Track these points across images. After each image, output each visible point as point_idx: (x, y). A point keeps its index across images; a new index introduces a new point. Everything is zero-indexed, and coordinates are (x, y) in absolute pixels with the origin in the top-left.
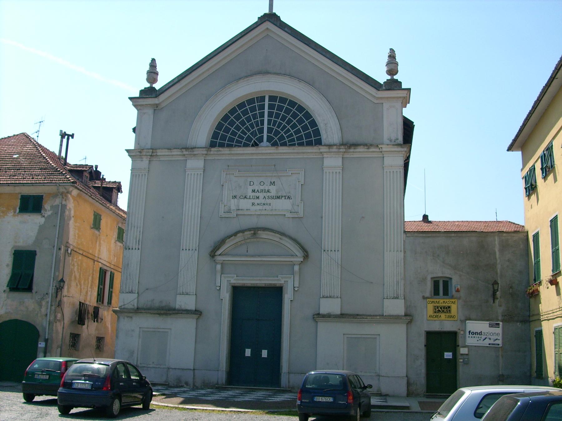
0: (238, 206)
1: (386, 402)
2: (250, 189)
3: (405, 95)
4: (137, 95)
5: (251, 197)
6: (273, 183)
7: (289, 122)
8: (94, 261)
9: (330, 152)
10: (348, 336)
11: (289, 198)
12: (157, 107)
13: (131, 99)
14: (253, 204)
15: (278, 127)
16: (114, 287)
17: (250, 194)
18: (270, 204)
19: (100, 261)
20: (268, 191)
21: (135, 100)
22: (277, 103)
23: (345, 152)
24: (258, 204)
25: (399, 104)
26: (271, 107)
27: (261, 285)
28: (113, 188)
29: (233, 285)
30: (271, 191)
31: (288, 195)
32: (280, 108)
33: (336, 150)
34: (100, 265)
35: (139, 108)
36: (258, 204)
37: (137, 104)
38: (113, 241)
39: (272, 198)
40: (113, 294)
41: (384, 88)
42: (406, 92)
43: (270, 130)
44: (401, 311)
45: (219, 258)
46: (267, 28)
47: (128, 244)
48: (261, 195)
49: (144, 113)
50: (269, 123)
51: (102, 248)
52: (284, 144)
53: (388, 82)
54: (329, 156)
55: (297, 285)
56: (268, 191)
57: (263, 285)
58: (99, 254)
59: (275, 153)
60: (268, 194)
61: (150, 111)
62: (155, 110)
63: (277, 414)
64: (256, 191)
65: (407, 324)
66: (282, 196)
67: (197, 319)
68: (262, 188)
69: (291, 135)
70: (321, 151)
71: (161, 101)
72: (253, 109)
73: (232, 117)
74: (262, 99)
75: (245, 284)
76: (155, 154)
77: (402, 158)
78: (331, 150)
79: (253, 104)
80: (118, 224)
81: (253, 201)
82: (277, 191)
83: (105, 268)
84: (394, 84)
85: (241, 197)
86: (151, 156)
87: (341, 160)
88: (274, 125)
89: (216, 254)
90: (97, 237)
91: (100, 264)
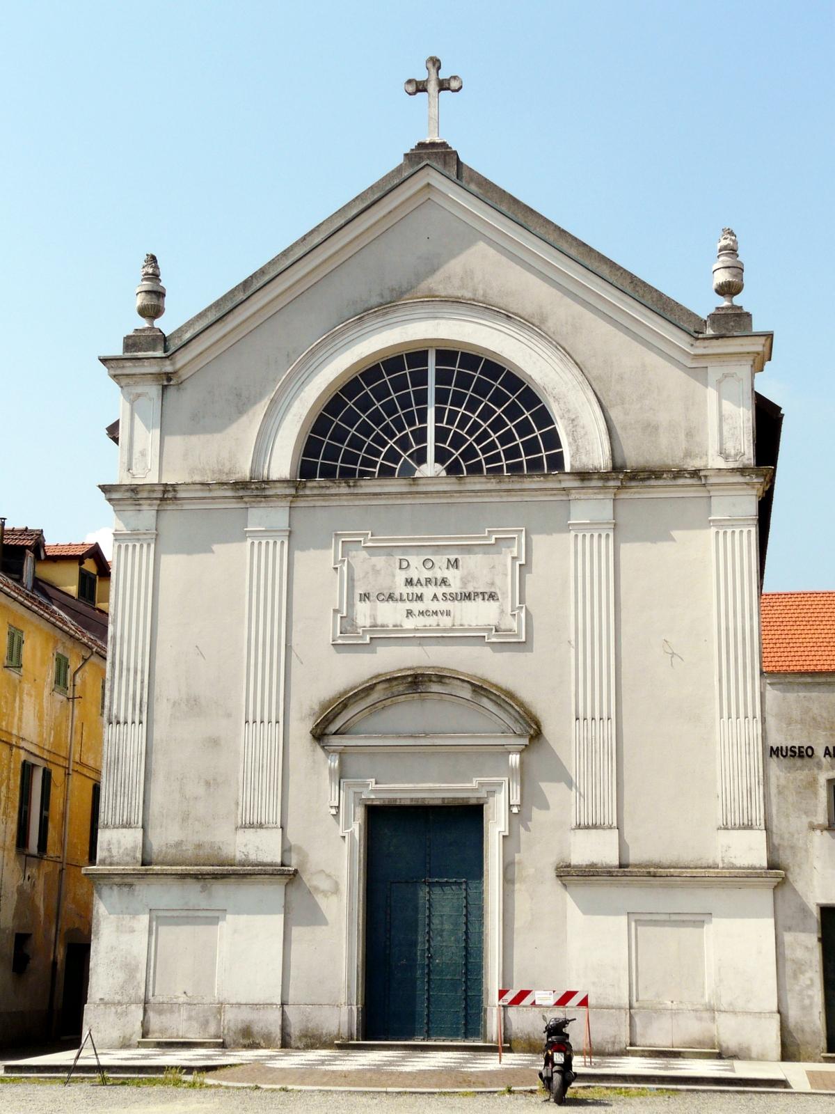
0: (374, 617)
1: (733, 1070)
2: (401, 577)
3: (759, 348)
4: (118, 351)
5: (405, 597)
6: (455, 564)
7: (486, 414)
8: (11, 746)
9: (583, 488)
10: (638, 917)
11: (492, 596)
12: (169, 379)
13: (104, 361)
14: (409, 613)
15: (461, 426)
16: (50, 809)
17: (401, 589)
18: (448, 613)
19: (22, 744)
20: (444, 581)
21: (113, 364)
22: (456, 369)
23: (619, 488)
24: (421, 613)
25: (744, 370)
26: (442, 378)
27: (432, 803)
28: (25, 547)
29: (369, 803)
30: (451, 580)
31: (488, 590)
32: (464, 381)
33: (600, 484)
34: (23, 756)
35: (124, 381)
36: (421, 613)
37: (119, 372)
38: (47, 691)
39: (454, 597)
40: (50, 825)
41: (710, 332)
42: (762, 340)
43: (441, 434)
44: (760, 858)
45: (336, 741)
46: (429, 185)
47: (114, 711)
48: (428, 592)
49: (139, 395)
50: (439, 418)
51: (25, 712)
52: (475, 470)
53: (719, 318)
54: (583, 497)
55: (516, 800)
56: (444, 581)
57: (439, 802)
58: (19, 728)
59: (456, 492)
60: (444, 589)
61: (153, 390)
62: (164, 388)
63: (484, 1051)
64: (415, 581)
65: (775, 888)
66: (477, 594)
67: (286, 885)
68: (429, 574)
69: (492, 446)
70: (564, 485)
71: (178, 365)
72: (400, 384)
73: (351, 404)
74: (424, 354)
75: (395, 800)
76: (170, 495)
77: (754, 497)
78: (587, 484)
79: (401, 367)
80: (55, 648)
81: (408, 605)
82: (464, 582)
83: (32, 760)
84: (732, 322)
85: (382, 597)
86: (162, 499)
87: (610, 504)
88: (450, 422)
89: (327, 731)
90: (15, 687)
91: (22, 752)
